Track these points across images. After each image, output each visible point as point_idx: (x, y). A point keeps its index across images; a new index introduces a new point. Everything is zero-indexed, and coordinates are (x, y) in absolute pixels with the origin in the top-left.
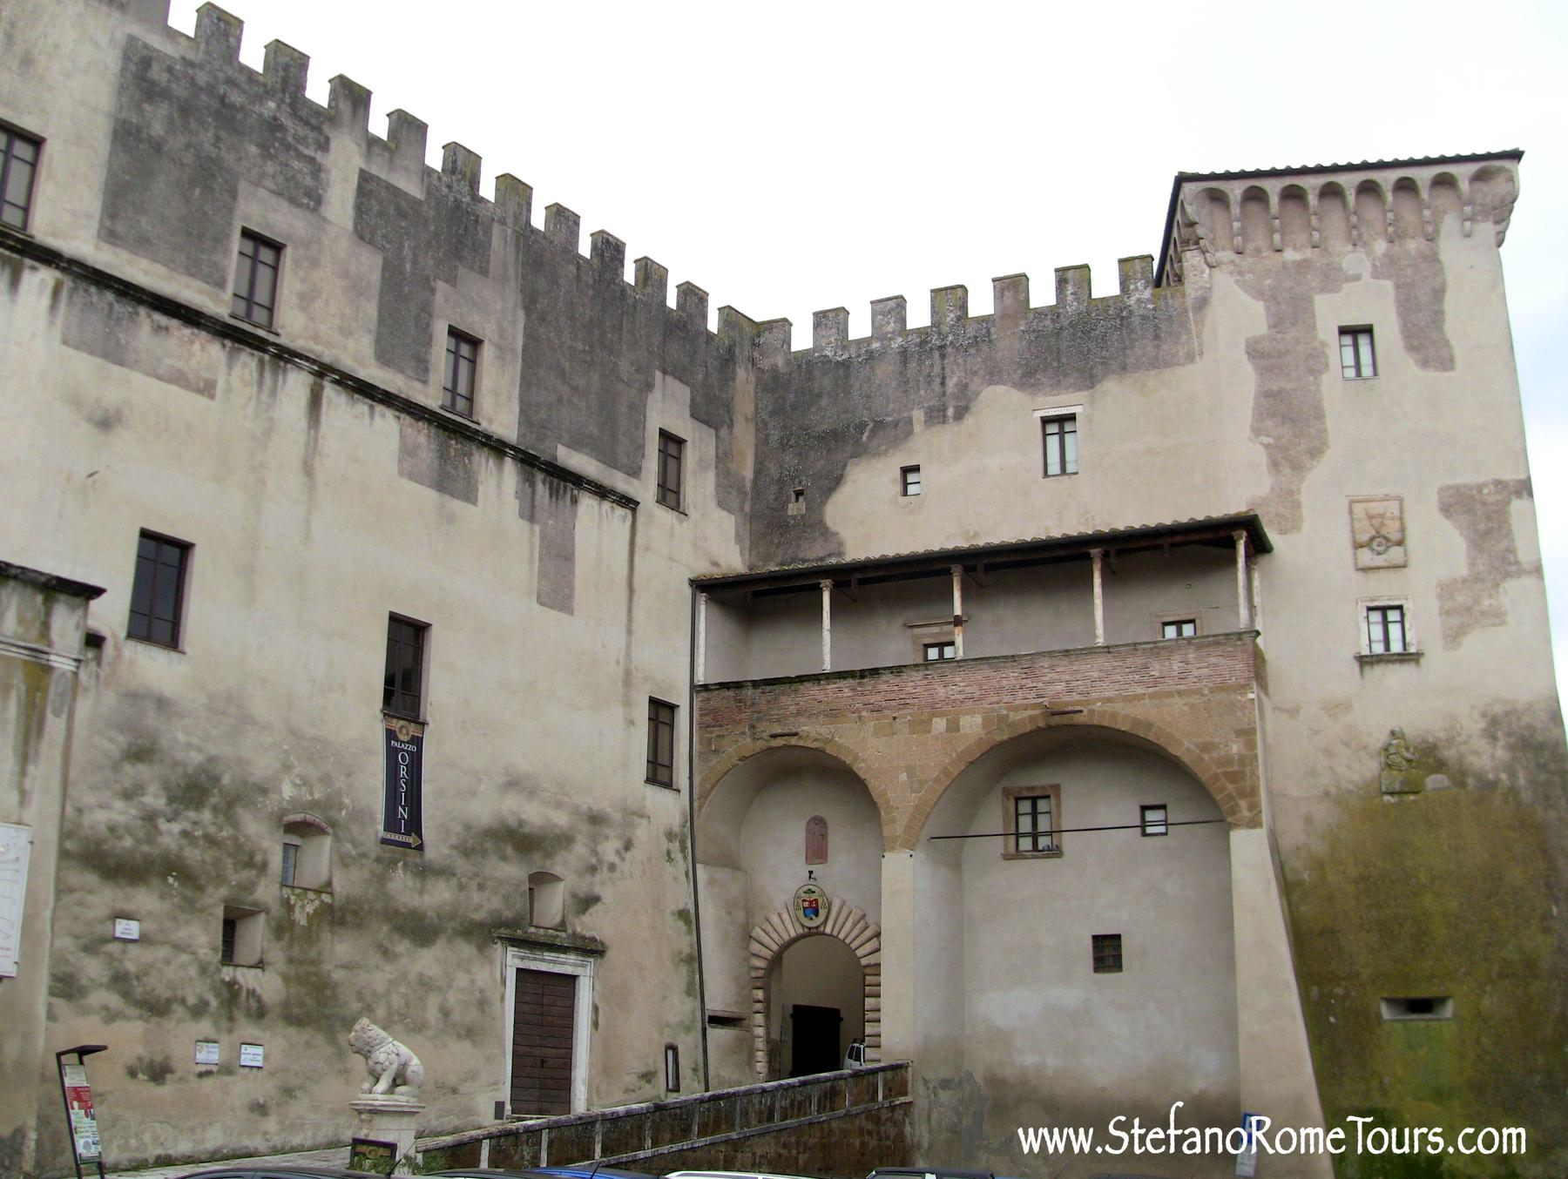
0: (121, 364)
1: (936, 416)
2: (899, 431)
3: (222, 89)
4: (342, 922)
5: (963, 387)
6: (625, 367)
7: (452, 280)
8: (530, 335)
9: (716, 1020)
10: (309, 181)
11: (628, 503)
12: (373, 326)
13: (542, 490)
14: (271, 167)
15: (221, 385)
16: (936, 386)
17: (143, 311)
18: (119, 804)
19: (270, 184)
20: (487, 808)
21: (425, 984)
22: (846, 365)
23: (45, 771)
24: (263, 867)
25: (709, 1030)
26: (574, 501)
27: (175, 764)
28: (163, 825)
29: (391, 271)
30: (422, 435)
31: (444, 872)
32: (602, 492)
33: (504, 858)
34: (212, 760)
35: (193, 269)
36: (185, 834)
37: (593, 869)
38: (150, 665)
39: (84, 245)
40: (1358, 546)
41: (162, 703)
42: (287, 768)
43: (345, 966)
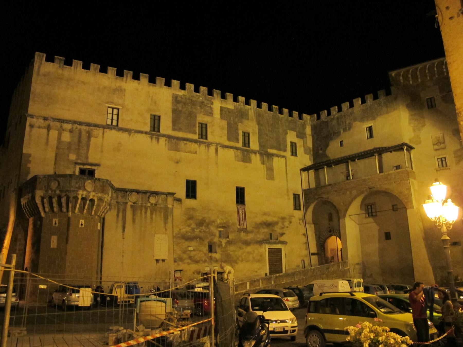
0: (179, 151)
1: (345, 130)
2: (338, 134)
3: (191, 98)
4: (231, 243)
5: (350, 123)
6: (281, 130)
7: (241, 123)
8: (260, 130)
9: (313, 254)
10: (210, 111)
11: (284, 157)
12: (227, 135)
13: (265, 158)
14: (202, 110)
15: (198, 152)
16: (344, 124)
17: (182, 141)
18: (187, 228)
19: (203, 113)
20: (260, 219)
21: (249, 253)
22: (327, 122)
23: (169, 225)
24: (215, 236)
25: (311, 256)
26: (273, 159)
27: (197, 219)
28: (196, 230)
29: (229, 125)
30: (239, 153)
31: (252, 232)
32: (278, 156)
33: (264, 228)
34: (203, 218)
35: (190, 132)
36: (200, 231)
37: (283, 228)
38: (191, 203)
39: (170, 132)
40: (434, 145)
41: (193, 209)
42: (218, 217)
43: (233, 251)
